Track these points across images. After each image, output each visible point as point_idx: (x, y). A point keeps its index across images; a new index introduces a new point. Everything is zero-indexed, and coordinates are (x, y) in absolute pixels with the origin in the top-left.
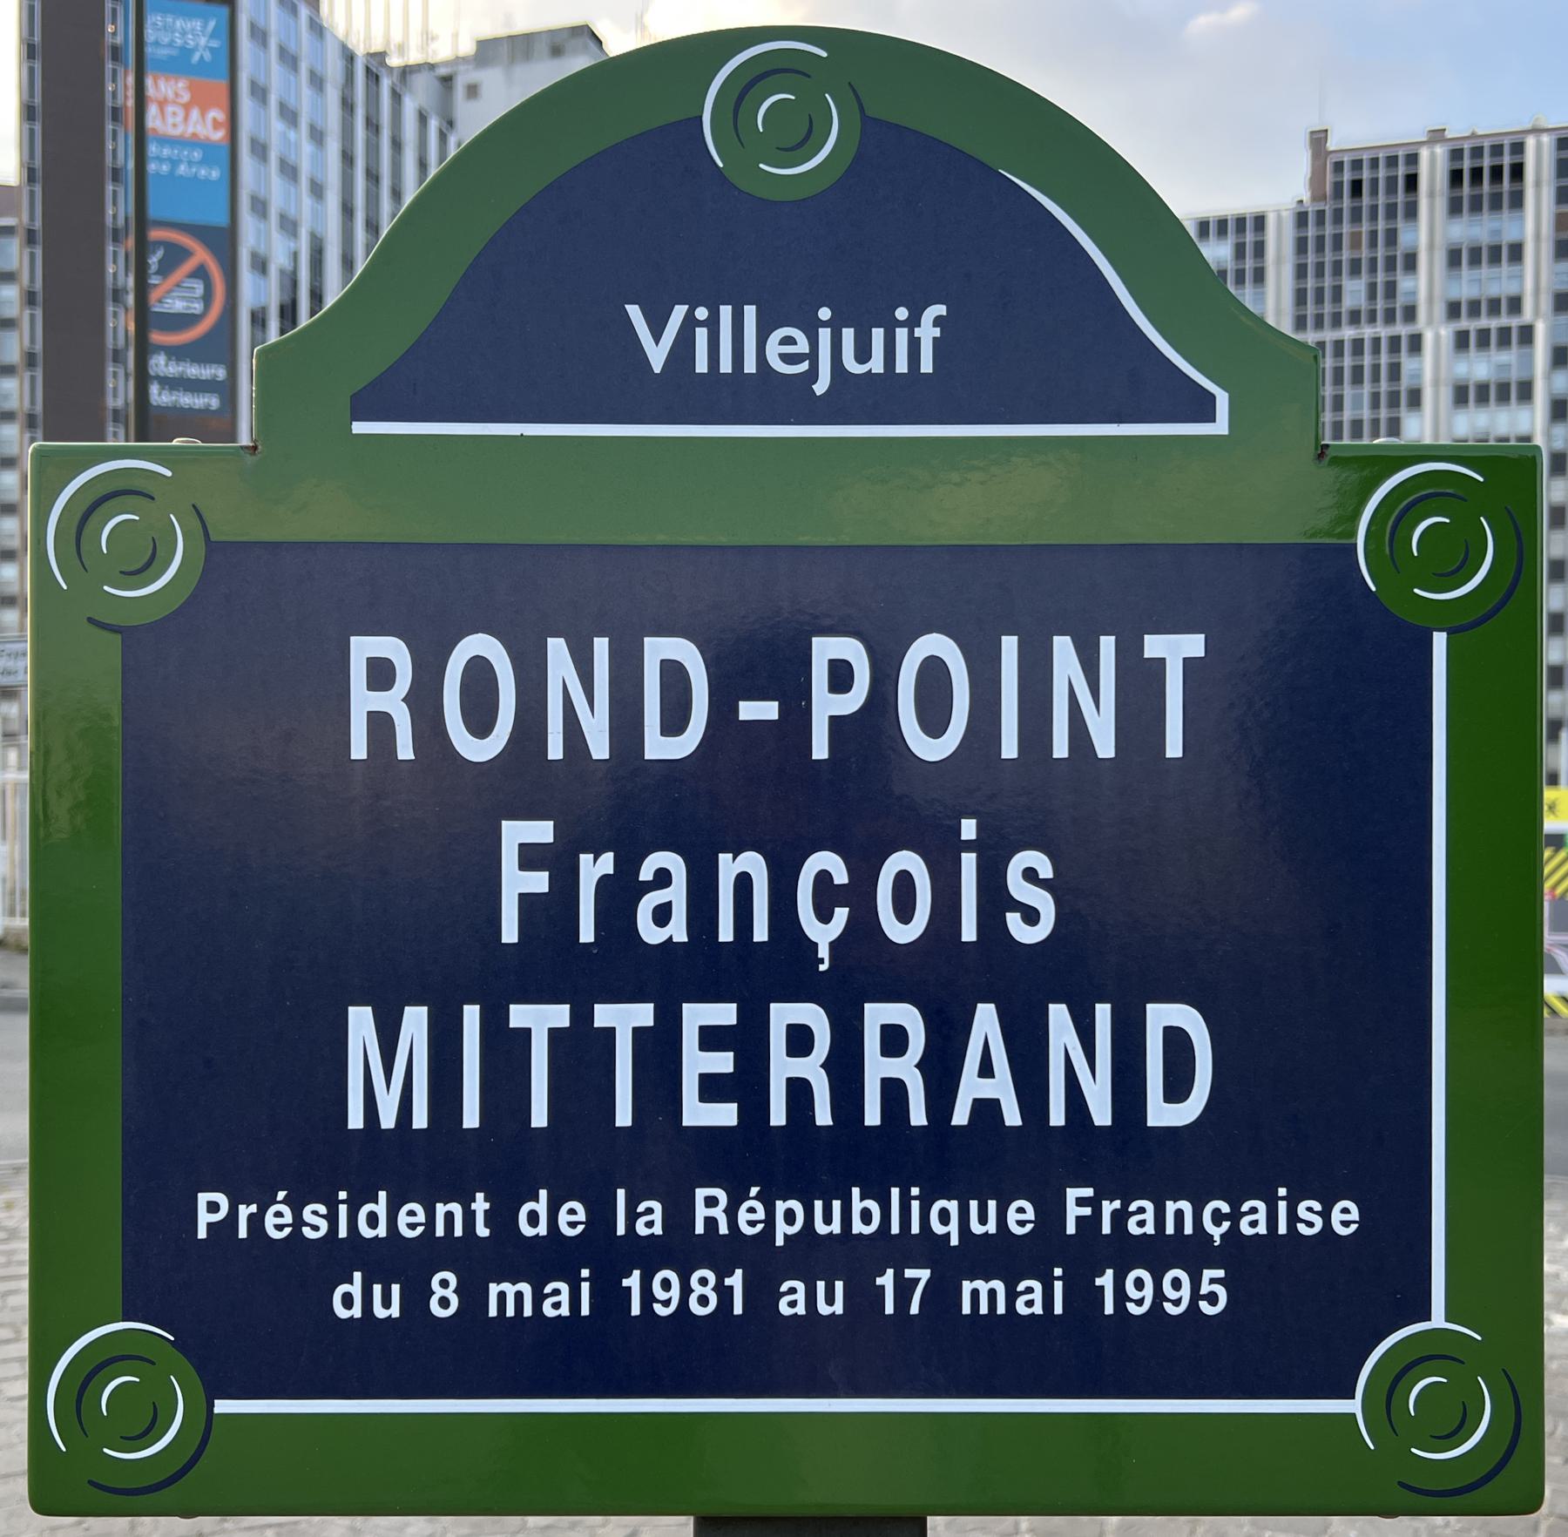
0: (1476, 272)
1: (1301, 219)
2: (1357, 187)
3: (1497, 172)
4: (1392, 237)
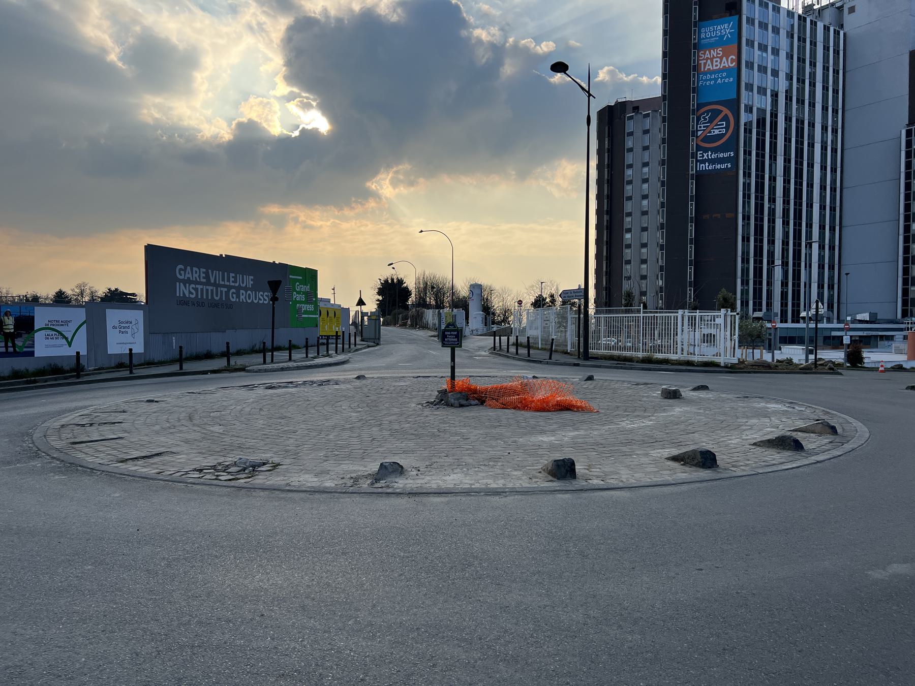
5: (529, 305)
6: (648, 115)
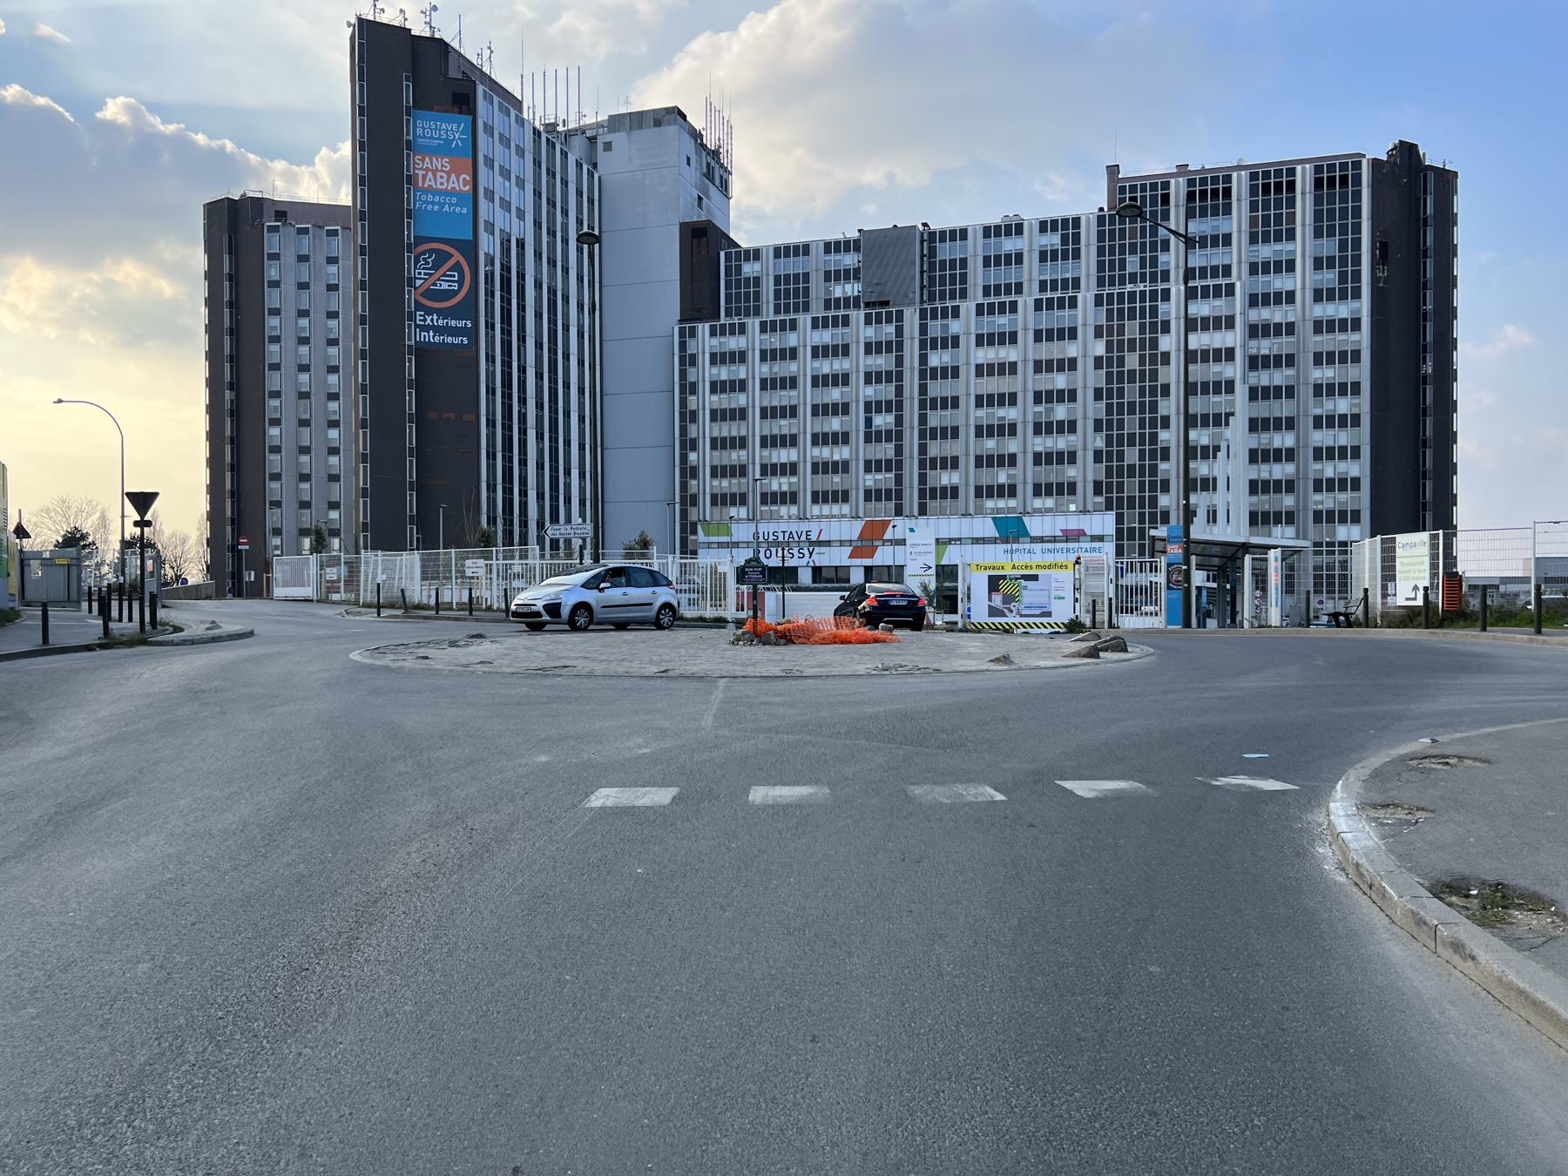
0: (1203, 252)
1: (1101, 220)
6: (304, 231)
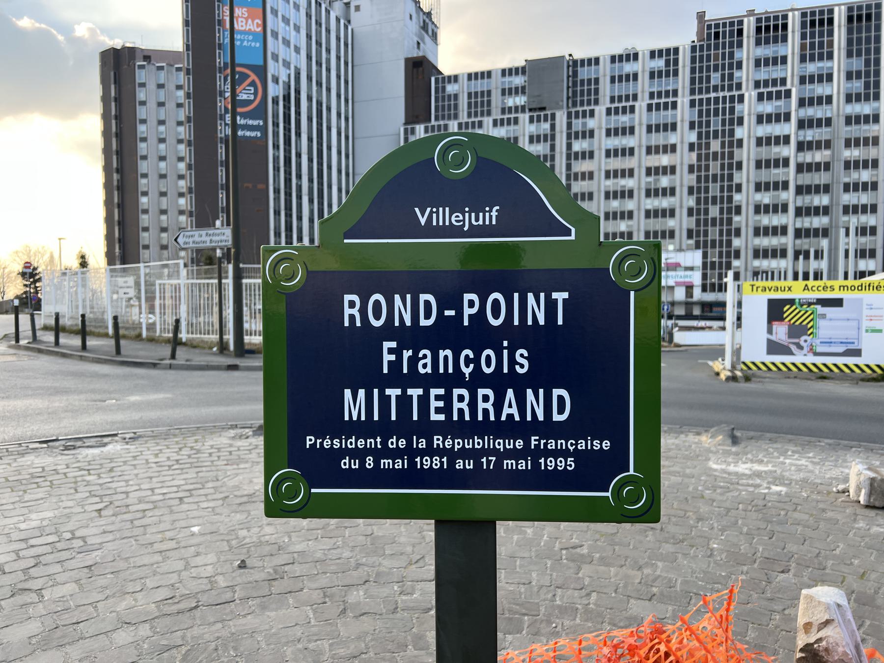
0: (767, 69)
1: (693, 49)
2: (717, 35)
3: (776, 27)
4: (731, 55)
5: (15, 274)
6: (161, 68)
